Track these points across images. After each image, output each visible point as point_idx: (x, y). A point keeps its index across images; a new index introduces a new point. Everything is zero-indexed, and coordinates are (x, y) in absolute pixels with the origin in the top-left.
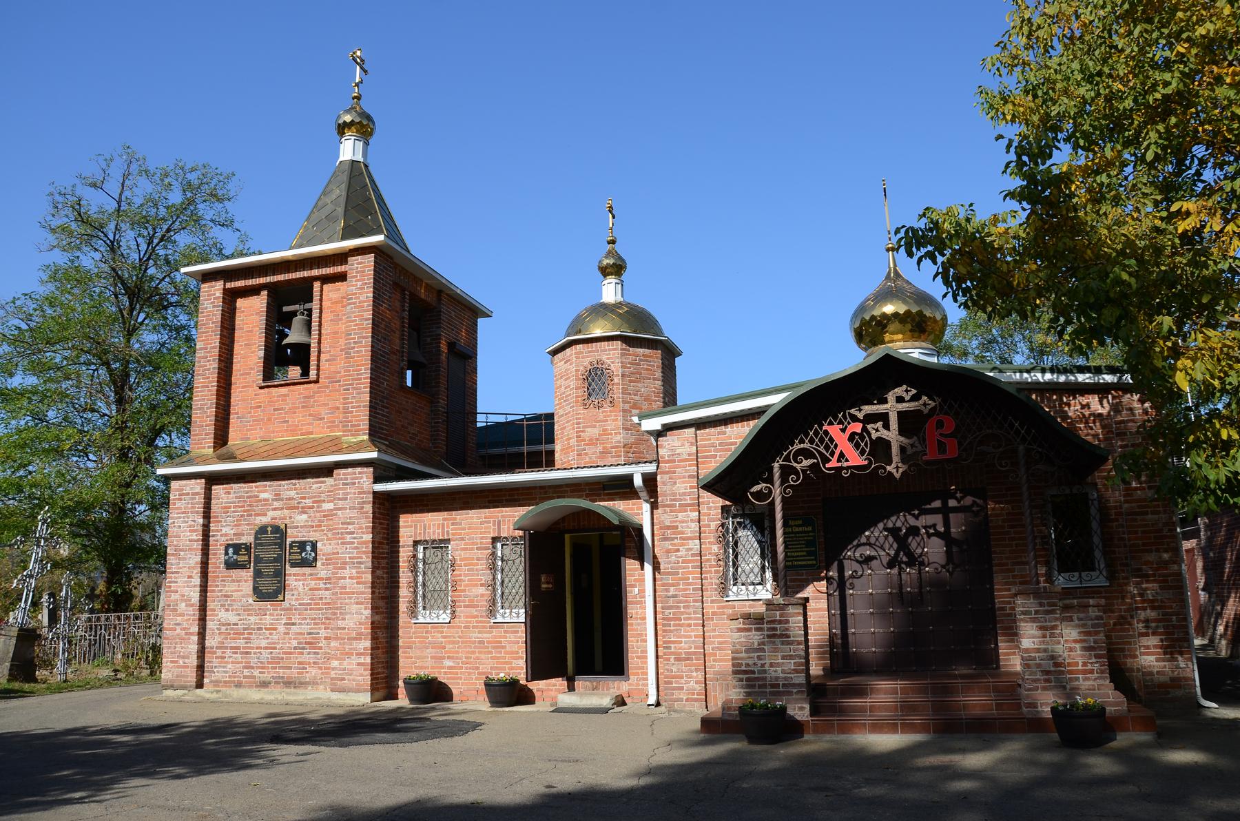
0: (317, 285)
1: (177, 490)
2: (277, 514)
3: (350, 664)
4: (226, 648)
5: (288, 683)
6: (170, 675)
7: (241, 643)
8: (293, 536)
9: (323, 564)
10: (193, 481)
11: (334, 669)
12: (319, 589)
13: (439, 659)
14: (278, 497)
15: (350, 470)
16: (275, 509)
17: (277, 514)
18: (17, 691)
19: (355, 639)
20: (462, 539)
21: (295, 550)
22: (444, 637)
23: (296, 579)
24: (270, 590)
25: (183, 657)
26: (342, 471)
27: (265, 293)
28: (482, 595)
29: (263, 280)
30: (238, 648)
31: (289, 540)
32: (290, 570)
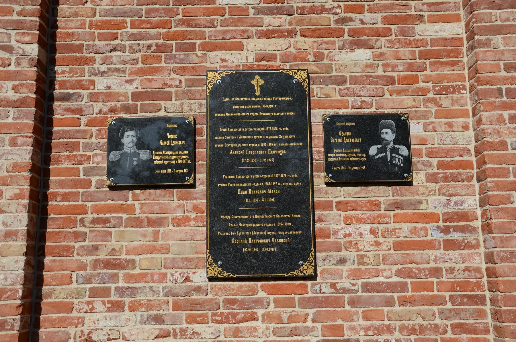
12: (430, 245)
16: (269, 34)
17: (275, 46)
21: (345, 137)
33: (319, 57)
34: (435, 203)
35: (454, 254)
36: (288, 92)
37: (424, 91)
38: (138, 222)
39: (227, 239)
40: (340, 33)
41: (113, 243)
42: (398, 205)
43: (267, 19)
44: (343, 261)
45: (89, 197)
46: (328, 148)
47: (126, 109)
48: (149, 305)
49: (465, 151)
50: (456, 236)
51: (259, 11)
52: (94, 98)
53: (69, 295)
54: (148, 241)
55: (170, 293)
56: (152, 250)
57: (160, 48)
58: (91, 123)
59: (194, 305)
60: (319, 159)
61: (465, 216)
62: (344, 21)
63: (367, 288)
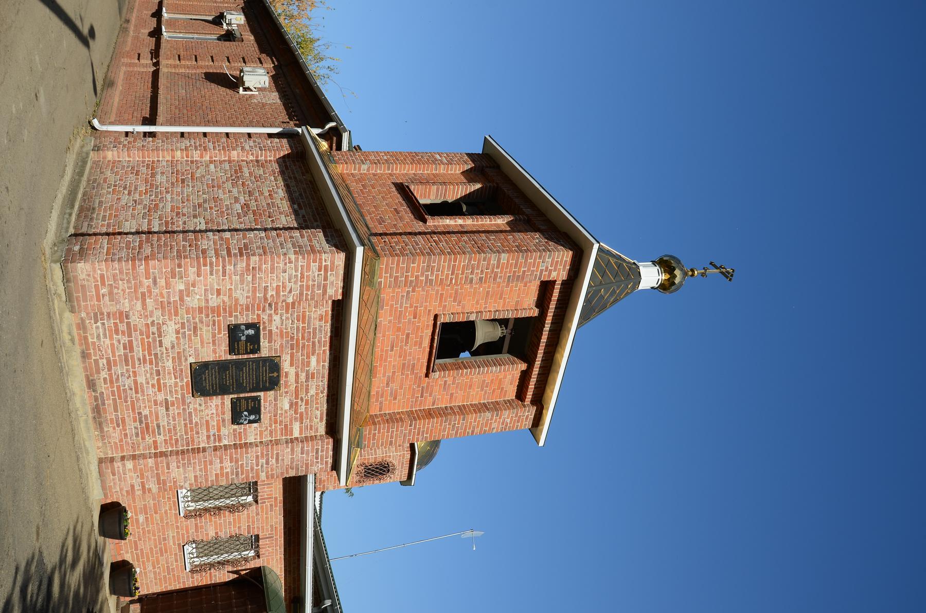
0: (524, 366)
1: (333, 263)
2: (292, 378)
3: (131, 478)
4: (130, 335)
5: (98, 410)
6: (82, 276)
7: (138, 352)
9: (235, 430)
10: (341, 284)
11: (124, 465)
12: (208, 430)
13: (145, 510)
14: (310, 376)
15: (331, 453)
16: (297, 375)
17: (292, 378)
18: (75, 541)
19: (158, 480)
20: (257, 514)
21: (251, 404)
22: (166, 512)
24: (205, 379)
25: (111, 293)
26: (331, 447)
27: (535, 312)
28: (207, 534)
29: (549, 319)
30: (132, 349)
31: (262, 394)
32: (228, 399)
33: (287, 392)
34: (224, 431)
35: (205, 438)
36: (273, 384)
37: (271, 426)
38: (214, 336)
39: (208, 369)
40: (297, 398)
41: (205, 328)
42: (224, 420)
43: (304, 374)
44: (200, 405)
45: (225, 317)
46: (246, 399)
47: (264, 328)
48: (178, 344)
50: (212, 438)
51: (308, 371)
52: (270, 315)
53: (182, 315)
54: (206, 341)
55: (184, 350)
56: (202, 342)
57: (292, 338)
58: (258, 316)
59: (180, 359)
60: (242, 395)
61: (220, 440)
62: (302, 399)
63: (190, 413)
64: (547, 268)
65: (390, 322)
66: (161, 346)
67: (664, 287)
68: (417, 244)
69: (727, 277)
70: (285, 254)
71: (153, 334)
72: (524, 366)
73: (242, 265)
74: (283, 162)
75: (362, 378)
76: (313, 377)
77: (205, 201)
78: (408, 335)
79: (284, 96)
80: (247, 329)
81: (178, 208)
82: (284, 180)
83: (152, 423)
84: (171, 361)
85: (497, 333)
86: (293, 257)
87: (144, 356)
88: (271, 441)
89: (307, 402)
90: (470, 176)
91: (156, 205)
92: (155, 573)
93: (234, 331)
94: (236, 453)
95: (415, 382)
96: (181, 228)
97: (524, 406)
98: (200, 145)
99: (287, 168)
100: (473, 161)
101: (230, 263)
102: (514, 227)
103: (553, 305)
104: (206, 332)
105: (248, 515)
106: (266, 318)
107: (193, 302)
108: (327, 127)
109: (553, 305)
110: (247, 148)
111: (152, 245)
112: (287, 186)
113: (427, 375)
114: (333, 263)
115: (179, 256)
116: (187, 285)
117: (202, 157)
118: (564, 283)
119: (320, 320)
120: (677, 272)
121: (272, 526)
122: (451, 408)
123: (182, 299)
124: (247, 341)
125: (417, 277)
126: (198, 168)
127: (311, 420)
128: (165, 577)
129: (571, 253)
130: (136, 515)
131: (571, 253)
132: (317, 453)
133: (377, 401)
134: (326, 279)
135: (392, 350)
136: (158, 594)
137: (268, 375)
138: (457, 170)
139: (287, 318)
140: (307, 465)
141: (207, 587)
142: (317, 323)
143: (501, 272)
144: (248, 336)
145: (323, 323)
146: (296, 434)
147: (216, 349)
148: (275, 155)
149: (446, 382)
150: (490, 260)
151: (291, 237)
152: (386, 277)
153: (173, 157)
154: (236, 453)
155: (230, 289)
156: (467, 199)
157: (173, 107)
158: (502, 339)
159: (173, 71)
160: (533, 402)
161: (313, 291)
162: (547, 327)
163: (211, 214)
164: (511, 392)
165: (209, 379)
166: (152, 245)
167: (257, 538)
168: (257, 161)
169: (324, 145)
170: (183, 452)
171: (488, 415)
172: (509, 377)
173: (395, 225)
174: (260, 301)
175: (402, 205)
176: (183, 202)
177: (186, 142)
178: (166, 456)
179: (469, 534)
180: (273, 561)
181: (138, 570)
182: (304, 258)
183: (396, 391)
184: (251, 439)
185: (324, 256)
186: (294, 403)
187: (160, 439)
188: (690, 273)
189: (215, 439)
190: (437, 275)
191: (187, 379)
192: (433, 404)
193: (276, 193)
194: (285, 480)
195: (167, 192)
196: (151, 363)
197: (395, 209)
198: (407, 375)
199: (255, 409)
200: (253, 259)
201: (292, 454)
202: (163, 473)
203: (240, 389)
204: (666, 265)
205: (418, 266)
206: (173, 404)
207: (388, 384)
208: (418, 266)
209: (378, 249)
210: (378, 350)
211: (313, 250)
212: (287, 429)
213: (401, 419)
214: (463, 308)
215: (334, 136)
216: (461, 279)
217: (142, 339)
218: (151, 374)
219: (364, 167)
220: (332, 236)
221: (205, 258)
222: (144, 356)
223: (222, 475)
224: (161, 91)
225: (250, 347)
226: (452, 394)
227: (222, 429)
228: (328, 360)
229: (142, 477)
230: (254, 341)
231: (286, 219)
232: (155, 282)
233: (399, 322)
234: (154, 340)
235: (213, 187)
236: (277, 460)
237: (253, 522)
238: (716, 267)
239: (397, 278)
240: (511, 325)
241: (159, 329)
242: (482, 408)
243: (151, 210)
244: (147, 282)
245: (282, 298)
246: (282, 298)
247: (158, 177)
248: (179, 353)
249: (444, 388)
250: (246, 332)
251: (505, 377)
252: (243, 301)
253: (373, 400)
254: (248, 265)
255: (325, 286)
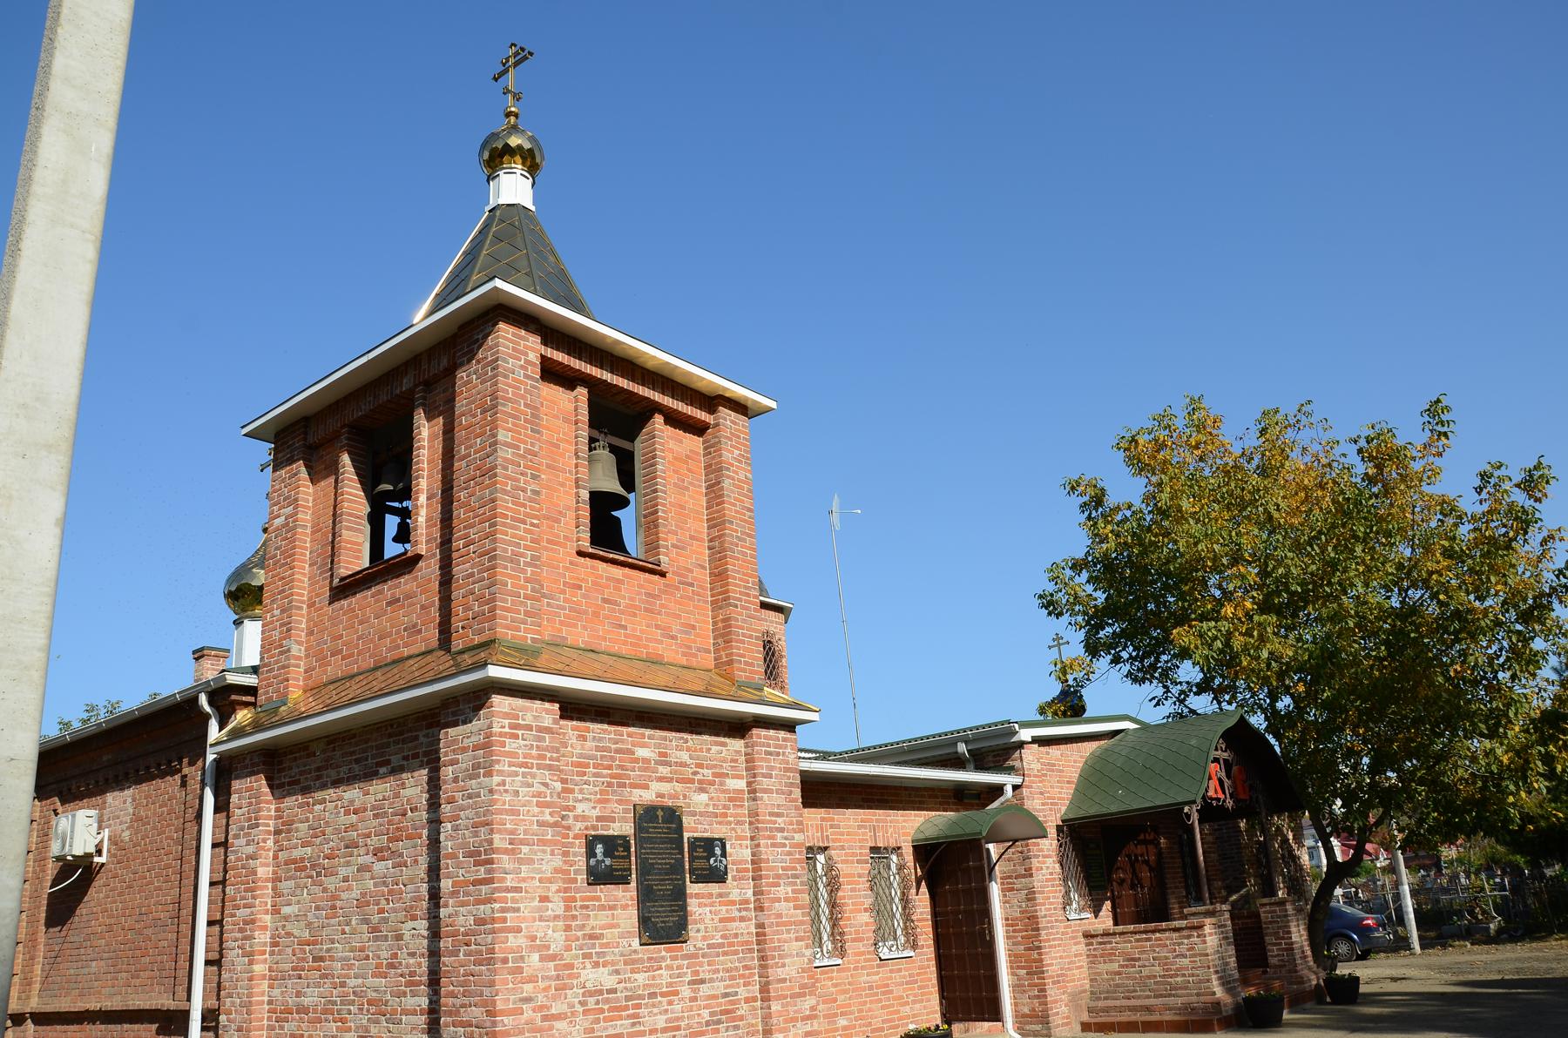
0: (658, 419)
1: (506, 715)
2: (665, 788)
8: (693, 828)
9: (734, 879)
10: (537, 704)
12: (732, 920)
14: (663, 759)
15: (772, 732)
16: (661, 779)
17: (665, 788)
20: (843, 848)
21: (700, 852)
22: (835, 985)
23: (704, 905)
24: (663, 924)
26: (763, 732)
27: (582, 392)
28: (867, 924)
31: (686, 835)
32: (692, 888)
33: (685, 797)
34: (735, 895)
36: (672, 817)
38: (602, 908)
40: (692, 781)
41: (592, 922)
42: (720, 895)
43: (661, 768)
45: (577, 890)
47: (595, 828)
48: (613, 963)
49: (746, 862)
51: (657, 763)
52: (576, 818)
54: (609, 921)
55: (622, 955)
57: (610, 785)
59: (634, 962)
61: (747, 902)
62: (695, 773)
63: (710, 946)
64: (522, 367)
65: (584, 627)
66: (614, 991)
67: (533, 168)
68: (472, 575)
69: (525, 58)
70: (491, 791)
71: (597, 1003)
72: (658, 419)
73: (505, 861)
74: (280, 788)
75: (662, 679)
76: (664, 755)
77: (367, 921)
78: (605, 601)
79: (119, 781)
80: (595, 855)
81: (378, 966)
82: (324, 787)
83: (720, 1005)
84: (636, 976)
85: (605, 456)
86: (496, 779)
87: (629, 1017)
88: (751, 823)
89: (698, 766)
90: (333, 469)
91: (370, 1003)
92: (914, 1002)
93: (598, 877)
94: (768, 877)
95: (672, 594)
96: (424, 962)
97: (717, 425)
98: (241, 930)
99: (297, 782)
100: (291, 461)
101: (503, 880)
102: (444, 408)
103: (577, 364)
104: (597, 920)
105: (843, 862)
106: (579, 825)
107: (556, 939)
108: (207, 708)
109: (577, 364)
110: (250, 849)
111: (463, 1006)
112: (336, 783)
113: (663, 574)
114: (506, 715)
115: (490, 962)
116: (533, 949)
117: (265, 928)
118: (545, 343)
119: (584, 739)
120: (514, 141)
121: (860, 827)
122: (711, 541)
123: (553, 958)
124: (612, 857)
125: (527, 580)
126: (289, 934)
127: (724, 761)
128: (920, 988)
129: (501, 325)
130: (837, 1030)
131: (501, 325)
132: (770, 754)
133: (695, 656)
134: (529, 728)
135: (625, 628)
136: (942, 997)
137: (660, 822)
138: (308, 492)
139: (581, 791)
140: (787, 770)
141: (936, 926)
142: (589, 744)
143: (525, 443)
144: (606, 854)
145: (590, 735)
146: (741, 784)
147: (620, 907)
148: (268, 802)
149: (674, 546)
150: (505, 459)
151: (456, 780)
152: (526, 630)
153: (263, 977)
154: (768, 877)
155: (541, 880)
156: (369, 481)
157: (137, 982)
158: (613, 449)
159: (37, 986)
160: (712, 410)
161: (546, 749)
162: (607, 376)
163: (395, 911)
164: (692, 443)
165: (664, 917)
166: (463, 1006)
167: (874, 849)
168: (277, 832)
169: (242, 716)
170: (762, 958)
171: (727, 483)
172: (671, 444)
173: (423, 607)
174: (558, 834)
175: (381, 592)
176: (367, 958)
177: (233, 955)
178: (768, 983)
179: (835, 518)
180: (906, 827)
181: (912, 1027)
182: (498, 762)
183: (683, 625)
184: (747, 854)
185: (496, 729)
186: (701, 784)
187: (743, 993)
188: (513, 119)
189: (746, 909)
190: (526, 547)
191: (661, 950)
192: (704, 568)
193: (352, 802)
194: (806, 804)
195: (343, 985)
196: (638, 1006)
197: (389, 604)
198: (662, 606)
199: (707, 846)
200: (497, 843)
201: (771, 791)
202: (791, 988)
203: (677, 869)
204: (496, 158)
205: (510, 576)
206: (696, 973)
207: (673, 637)
208: (510, 576)
209: (477, 640)
210: (625, 650)
211: (486, 746)
212: (735, 798)
213: (724, 621)
214: (569, 508)
215: (225, 697)
216: (532, 508)
217: (605, 1020)
218: (654, 1006)
219: (297, 650)
220: (454, 714)
221: (493, 920)
222: (629, 1017)
223: (796, 899)
224: (93, 1005)
225: (620, 852)
226: (692, 537)
227: (732, 897)
228: (642, 730)
229: (794, 1020)
230: (613, 844)
231: (414, 786)
232: (528, 1000)
233: (585, 612)
234: (607, 1001)
235: (333, 907)
236: (778, 815)
237: (854, 854)
238: (506, 71)
239: (527, 614)
240: (596, 434)
241: (591, 994)
242: (714, 492)
243: (378, 1008)
244: (528, 1014)
245: (555, 799)
246: (555, 799)
247: (306, 1001)
248: (626, 963)
249: (683, 548)
250: (600, 856)
251: (671, 450)
252: (558, 862)
253: (694, 662)
254: (506, 851)
255: (541, 729)
